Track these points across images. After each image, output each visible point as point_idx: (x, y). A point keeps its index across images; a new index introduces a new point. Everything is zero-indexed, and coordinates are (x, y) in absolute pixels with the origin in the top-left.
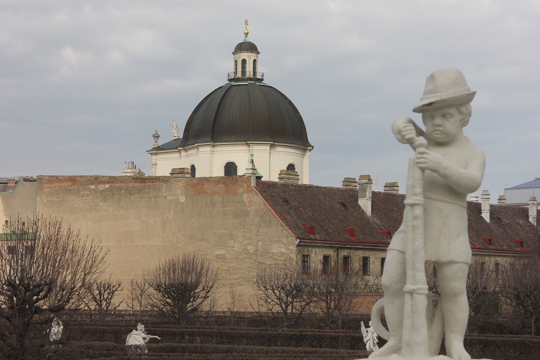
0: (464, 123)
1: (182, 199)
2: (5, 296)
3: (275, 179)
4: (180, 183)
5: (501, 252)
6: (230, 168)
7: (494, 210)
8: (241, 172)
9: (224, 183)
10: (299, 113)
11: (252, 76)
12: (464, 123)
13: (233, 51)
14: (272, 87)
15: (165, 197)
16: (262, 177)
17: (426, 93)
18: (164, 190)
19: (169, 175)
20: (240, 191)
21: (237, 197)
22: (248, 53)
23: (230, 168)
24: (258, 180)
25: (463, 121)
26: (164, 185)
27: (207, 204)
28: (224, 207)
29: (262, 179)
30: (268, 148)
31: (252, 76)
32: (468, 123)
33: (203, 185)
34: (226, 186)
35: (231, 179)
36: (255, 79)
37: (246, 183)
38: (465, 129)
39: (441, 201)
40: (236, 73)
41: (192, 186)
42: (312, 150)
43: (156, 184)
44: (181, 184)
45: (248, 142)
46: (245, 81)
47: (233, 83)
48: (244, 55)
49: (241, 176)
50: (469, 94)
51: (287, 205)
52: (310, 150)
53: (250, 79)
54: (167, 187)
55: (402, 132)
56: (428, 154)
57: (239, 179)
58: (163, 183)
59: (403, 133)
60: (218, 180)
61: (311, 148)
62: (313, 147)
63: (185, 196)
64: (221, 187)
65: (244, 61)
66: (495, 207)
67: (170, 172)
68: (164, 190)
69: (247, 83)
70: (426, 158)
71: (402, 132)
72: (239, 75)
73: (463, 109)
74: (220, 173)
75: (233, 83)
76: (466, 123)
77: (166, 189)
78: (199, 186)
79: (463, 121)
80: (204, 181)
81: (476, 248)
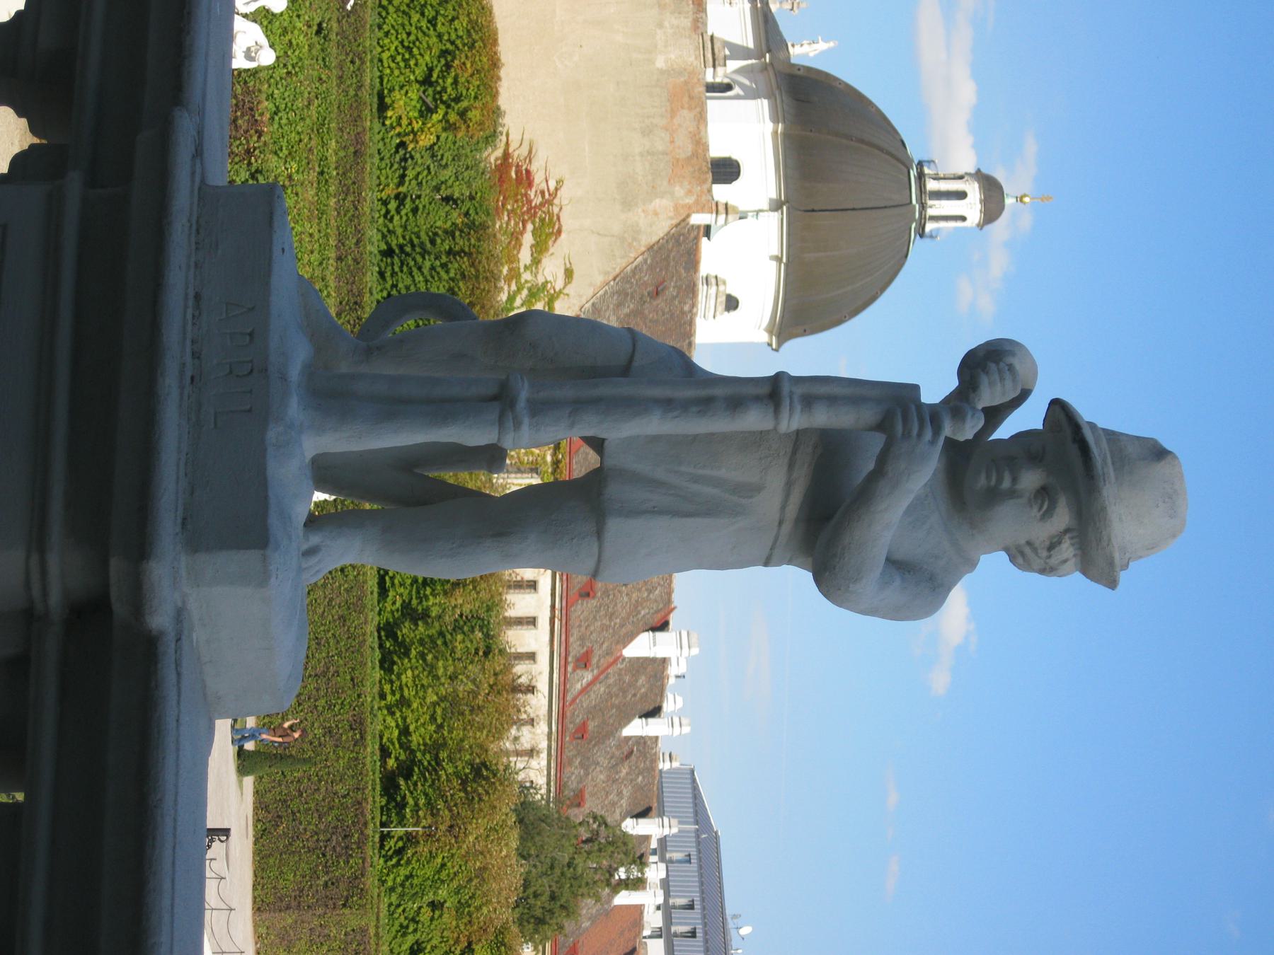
0: (1022, 554)
1: (660, 63)
2: (388, 803)
3: (705, 268)
4: (693, 57)
5: (560, 762)
6: (726, 170)
7: (646, 745)
8: (721, 192)
9: (695, 154)
10: (850, 319)
11: (930, 212)
12: (1022, 554)
13: (984, 171)
14: (906, 256)
15: (660, 26)
16: (709, 239)
17: (1112, 436)
18: (675, 22)
19: (710, 33)
20: (679, 191)
21: (665, 183)
22: (981, 203)
23: (726, 170)
24: (702, 229)
25: (1027, 550)
26: (687, 22)
27: (648, 117)
28: (641, 155)
29: (704, 240)
30: (776, 252)
31: (930, 212)
32: (1020, 567)
33: (690, 109)
34: (689, 159)
35: (705, 169)
36: (923, 221)
37: (697, 202)
38: (1002, 556)
39: (789, 485)
40: (936, 178)
41: (686, 83)
42: (770, 348)
43: (688, 5)
44: (692, 59)
45: (785, 208)
46: (919, 198)
47: (913, 173)
48: (974, 191)
49: (710, 191)
50: (1111, 564)
51: (649, 294)
52: (770, 345)
53: (923, 207)
54: (684, 28)
55: (997, 363)
56: (933, 442)
57: (705, 187)
58: (690, 19)
59: (993, 366)
60: (700, 143)
61: (774, 346)
62: (776, 350)
63: (664, 68)
64: (685, 147)
65: (961, 195)
66: (654, 746)
67: (715, 35)
68: (675, 22)
69: (914, 201)
70: (920, 435)
71: (997, 363)
72: (932, 185)
73: (1067, 549)
74: (717, 150)
75: (913, 173)
76: (1020, 560)
77: (678, 27)
78: (686, 99)
79: (1027, 550)
80: (698, 109)
81: (566, 709)
